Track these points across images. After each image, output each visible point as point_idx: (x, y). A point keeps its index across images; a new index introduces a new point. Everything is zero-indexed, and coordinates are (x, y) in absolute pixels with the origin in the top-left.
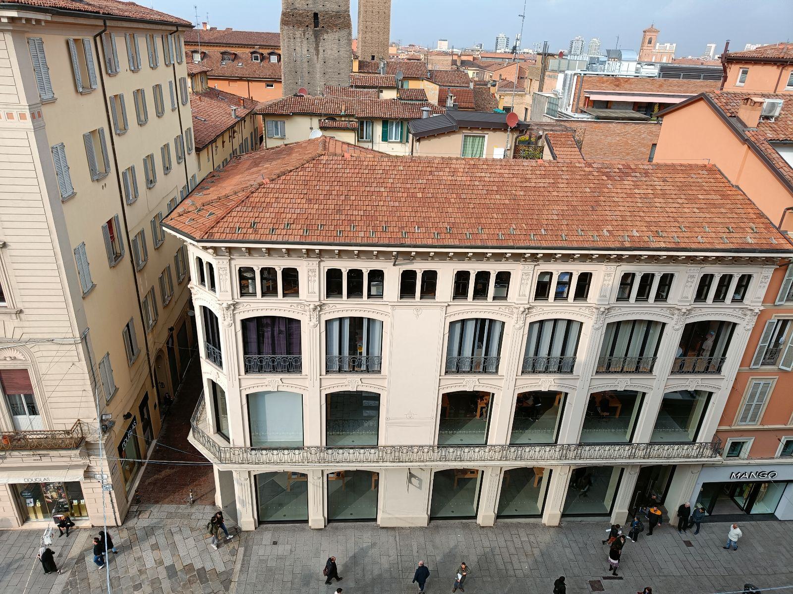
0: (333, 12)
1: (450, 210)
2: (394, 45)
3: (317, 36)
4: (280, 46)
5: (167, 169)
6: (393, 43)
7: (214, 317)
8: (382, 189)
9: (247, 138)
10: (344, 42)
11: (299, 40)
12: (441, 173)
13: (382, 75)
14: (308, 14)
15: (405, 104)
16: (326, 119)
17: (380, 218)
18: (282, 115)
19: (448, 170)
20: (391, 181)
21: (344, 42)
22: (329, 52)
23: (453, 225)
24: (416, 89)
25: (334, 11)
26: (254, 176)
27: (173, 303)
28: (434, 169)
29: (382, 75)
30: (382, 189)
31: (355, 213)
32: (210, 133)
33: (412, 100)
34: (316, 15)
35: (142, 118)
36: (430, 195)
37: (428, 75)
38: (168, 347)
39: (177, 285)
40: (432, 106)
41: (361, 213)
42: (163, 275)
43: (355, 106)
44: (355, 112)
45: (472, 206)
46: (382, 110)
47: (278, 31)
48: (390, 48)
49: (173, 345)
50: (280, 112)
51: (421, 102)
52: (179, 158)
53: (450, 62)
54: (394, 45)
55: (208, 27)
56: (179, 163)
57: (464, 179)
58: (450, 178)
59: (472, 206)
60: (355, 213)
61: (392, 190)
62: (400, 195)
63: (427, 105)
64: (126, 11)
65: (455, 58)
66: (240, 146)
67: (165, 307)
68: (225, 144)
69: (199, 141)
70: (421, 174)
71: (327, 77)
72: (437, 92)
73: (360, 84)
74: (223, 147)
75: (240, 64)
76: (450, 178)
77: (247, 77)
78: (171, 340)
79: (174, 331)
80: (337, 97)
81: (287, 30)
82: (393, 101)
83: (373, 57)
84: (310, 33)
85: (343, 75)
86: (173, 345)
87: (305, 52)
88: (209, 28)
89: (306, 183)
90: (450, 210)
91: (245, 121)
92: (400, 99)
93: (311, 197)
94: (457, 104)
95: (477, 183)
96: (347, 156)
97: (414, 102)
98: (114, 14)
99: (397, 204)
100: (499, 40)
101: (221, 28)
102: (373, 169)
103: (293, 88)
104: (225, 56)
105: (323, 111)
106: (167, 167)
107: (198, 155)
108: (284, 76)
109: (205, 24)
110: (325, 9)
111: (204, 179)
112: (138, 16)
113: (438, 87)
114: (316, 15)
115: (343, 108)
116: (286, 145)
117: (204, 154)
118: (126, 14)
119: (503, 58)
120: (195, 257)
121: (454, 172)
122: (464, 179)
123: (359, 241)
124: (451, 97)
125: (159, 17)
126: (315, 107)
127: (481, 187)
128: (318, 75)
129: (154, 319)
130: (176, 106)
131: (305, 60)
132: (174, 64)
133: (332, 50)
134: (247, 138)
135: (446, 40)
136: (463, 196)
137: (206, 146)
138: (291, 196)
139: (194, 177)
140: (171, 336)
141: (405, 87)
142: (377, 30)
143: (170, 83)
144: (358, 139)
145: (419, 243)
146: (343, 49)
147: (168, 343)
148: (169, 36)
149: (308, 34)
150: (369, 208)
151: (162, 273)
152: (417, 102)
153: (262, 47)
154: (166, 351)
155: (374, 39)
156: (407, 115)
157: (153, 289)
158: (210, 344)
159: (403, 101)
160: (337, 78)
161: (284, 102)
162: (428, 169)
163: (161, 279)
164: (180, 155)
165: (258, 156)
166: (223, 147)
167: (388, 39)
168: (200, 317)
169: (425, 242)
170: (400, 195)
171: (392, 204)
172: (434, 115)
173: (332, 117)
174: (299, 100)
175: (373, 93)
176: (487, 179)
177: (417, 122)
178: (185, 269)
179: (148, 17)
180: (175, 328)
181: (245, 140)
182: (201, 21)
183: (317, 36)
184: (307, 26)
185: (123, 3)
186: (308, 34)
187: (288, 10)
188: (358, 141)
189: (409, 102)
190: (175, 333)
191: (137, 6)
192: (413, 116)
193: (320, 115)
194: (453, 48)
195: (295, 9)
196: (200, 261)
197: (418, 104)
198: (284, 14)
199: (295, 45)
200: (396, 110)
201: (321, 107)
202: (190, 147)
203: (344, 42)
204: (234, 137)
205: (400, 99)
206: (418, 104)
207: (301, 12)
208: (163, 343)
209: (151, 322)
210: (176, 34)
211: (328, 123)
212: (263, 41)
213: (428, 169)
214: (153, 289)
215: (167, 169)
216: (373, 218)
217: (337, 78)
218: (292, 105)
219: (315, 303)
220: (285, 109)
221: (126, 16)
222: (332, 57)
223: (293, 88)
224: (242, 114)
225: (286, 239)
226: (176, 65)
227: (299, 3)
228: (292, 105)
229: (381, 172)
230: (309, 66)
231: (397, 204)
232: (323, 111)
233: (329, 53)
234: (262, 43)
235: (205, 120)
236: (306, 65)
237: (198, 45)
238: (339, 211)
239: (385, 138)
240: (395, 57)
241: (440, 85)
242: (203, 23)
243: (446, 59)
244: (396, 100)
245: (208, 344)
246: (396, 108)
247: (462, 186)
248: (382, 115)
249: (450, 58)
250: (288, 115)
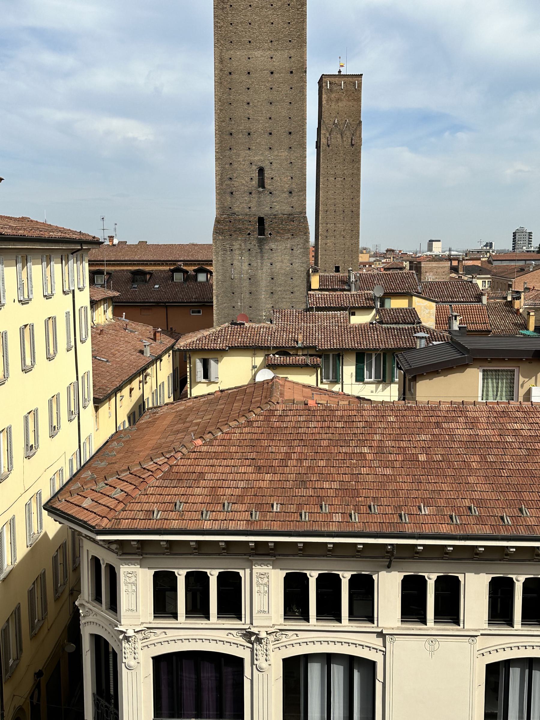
0: (284, 215)
1: (471, 480)
2: (364, 251)
3: (261, 243)
4: (212, 261)
5: (54, 430)
6: (365, 249)
7: (111, 650)
8: (365, 450)
9: (163, 383)
10: (299, 251)
11: (237, 252)
12: (452, 425)
13: (353, 292)
14: (251, 219)
15: (388, 330)
16: (277, 354)
17: (364, 493)
18: (214, 350)
19: (461, 420)
20: (377, 437)
21: (298, 251)
22: (278, 265)
23: (480, 503)
24: (403, 309)
25: (285, 213)
26: (180, 436)
27: (45, 630)
28: (440, 419)
29: (353, 292)
30: (365, 450)
31: (326, 485)
32: (114, 378)
33: (399, 323)
34: (261, 220)
35: (28, 362)
36: (439, 458)
37: (419, 288)
38: (32, 703)
39: (53, 601)
40: (428, 330)
41: (335, 485)
42: (34, 586)
43: (317, 334)
44: (317, 342)
45: (505, 473)
46: (355, 338)
47: (210, 242)
48: (360, 255)
49: (39, 700)
50: (212, 346)
51: (412, 326)
52: (71, 413)
53: (447, 269)
54: (364, 251)
55: (116, 242)
56: (70, 420)
57: (488, 432)
58: (466, 432)
59: (505, 473)
60: (326, 485)
61: (380, 451)
62: (392, 457)
63: (420, 329)
64: (19, 229)
65: (455, 263)
66: (153, 393)
67: (33, 637)
68: (133, 392)
69: (99, 389)
70: (422, 428)
71: (276, 296)
72: (434, 311)
73: (323, 305)
74: (131, 396)
75: (157, 286)
76: (466, 432)
77: (165, 303)
78: (36, 692)
79: (42, 678)
80: (337, 324)
81: (222, 239)
82: (371, 325)
83: (337, 269)
84: (253, 243)
85: (297, 294)
86: (39, 700)
87: (245, 267)
88: (117, 242)
89: (253, 444)
90: (471, 480)
91: (161, 361)
92: (381, 322)
93: (260, 463)
94: (463, 326)
95: (509, 439)
96: (311, 403)
97: (401, 326)
98: (6, 234)
99: (388, 471)
100: (517, 236)
101: (132, 241)
102: (349, 421)
103: (228, 315)
104: (138, 277)
105: (272, 343)
106: (55, 427)
107: (97, 409)
108: (217, 298)
109: (111, 238)
110: (274, 211)
111: (107, 442)
112: (35, 234)
113: (434, 304)
114: (261, 220)
115: (300, 337)
116: (222, 391)
117: (104, 409)
118: (21, 232)
119: (525, 260)
120: (90, 557)
121: (473, 423)
122: (488, 432)
123: (333, 528)
124: (456, 316)
125: (59, 234)
126: (261, 337)
127: (517, 445)
128: (263, 296)
129: (15, 657)
130: (73, 344)
131: (245, 276)
132: (73, 291)
133: (282, 261)
134: (163, 383)
135: (439, 241)
136: (491, 458)
137: (108, 398)
138: (232, 463)
139: (89, 438)
140: (37, 686)
141: (387, 306)
142: (342, 233)
143: (68, 313)
144: (321, 379)
145: (427, 530)
146: (297, 261)
147: (32, 697)
148: (70, 256)
149: (250, 243)
150: (347, 478)
151: (34, 584)
152: (406, 326)
153: (187, 263)
154: (28, 710)
155: (338, 245)
156: (391, 344)
157: (18, 608)
158: (102, 697)
159: (385, 325)
160: (289, 298)
161: (217, 333)
162: (433, 420)
163: (31, 593)
164: (72, 409)
165: (183, 407)
166: (131, 396)
167: (358, 243)
168: (89, 654)
169: (435, 530)
170: (392, 457)
171: (379, 470)
172: (435, 343)
173: (283, 351)
174: (239, 329)
175: (342, 316)
176: (524, 433)
177: (408, 355)
178: (66, 577)
179: (46, 235)
180: (44, 673)
181: (160, 386)
182: (108, 234)
183: (261, 243)
184: (249, 234)
185: (15, 219)
186: (250, 243)
187: (223, 217)
188: (322, 382)
189: (394, 326)
190: (43, 680)
191: (32, 221)
192: (401, 345)
193: (268, 348)
194: (450, 250)
195: (233, 213)
196: (96, 562)
197: (407, 328)
198: (218, 221)
199: (232, 259)
200: (376, 338)
201: (270, 338)
202: (86, 397)
203: (299, 251)
204: (146, 383)
205: (381, 322)
206: (407, 328)
207: (240, 217)
208: (26, 696)
209: (11, 662)
210: (79, 253)
211: (278, 359)
212: (188, 256)
213: (433, 420)
214: (18, 608)
215: (54, 430)
216: (355, 493)
217: (289, 298)
218: (228, 337)
219: (267, 629)
220: (219, 342)
221: (21, 235)
222: (283, 271)
223: (228, 315)
224: (158, 351)
225: (224, 526)
226: (77, 291)
227: (238, 207)
228: (228, 337)
229: (361, 424)
230: (251, 284)
231: (388, 471)
232: (272, 343)
233: (278, 268)
234: (186, 258)
235: (107, 361)
236: (246, 283)
237: (106, 261)
238: (303, 483)
239: (360, 378)
240: (367, 266)
241: (437, 302)
242: (109, 237)
243: (441, 265)
244: (375, 324)
245: (99, 698)
246: (376, 336)
247: (487, 444)
248: (356, 345)
249: (448, 264)
250: (224, 350)
